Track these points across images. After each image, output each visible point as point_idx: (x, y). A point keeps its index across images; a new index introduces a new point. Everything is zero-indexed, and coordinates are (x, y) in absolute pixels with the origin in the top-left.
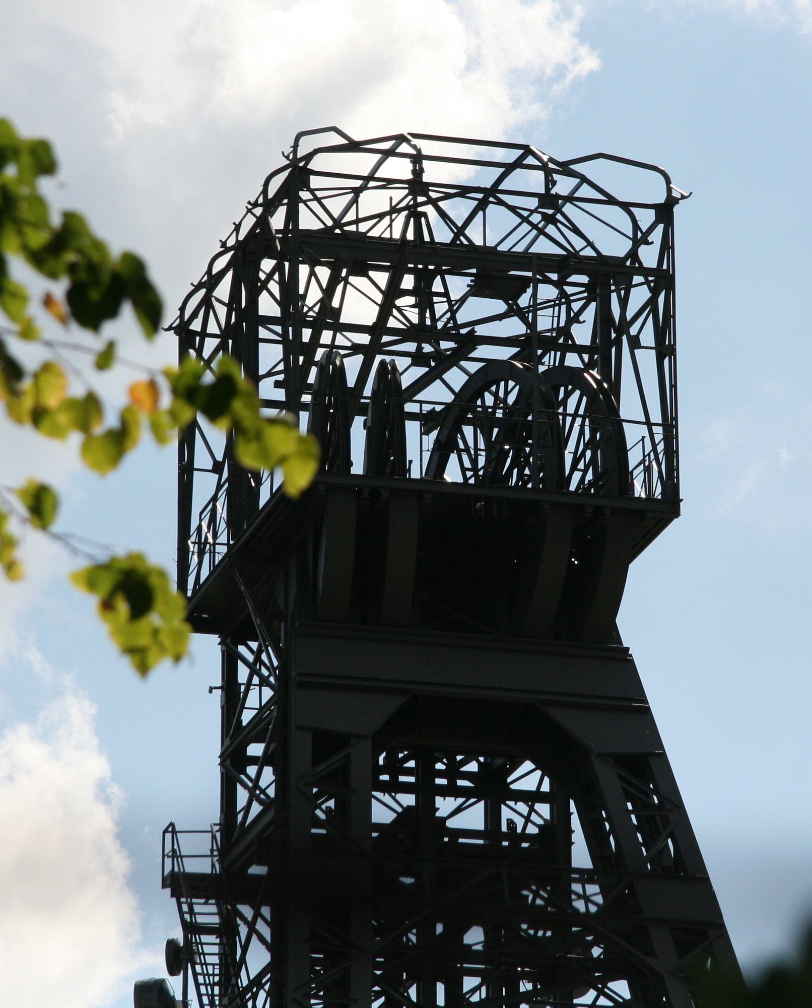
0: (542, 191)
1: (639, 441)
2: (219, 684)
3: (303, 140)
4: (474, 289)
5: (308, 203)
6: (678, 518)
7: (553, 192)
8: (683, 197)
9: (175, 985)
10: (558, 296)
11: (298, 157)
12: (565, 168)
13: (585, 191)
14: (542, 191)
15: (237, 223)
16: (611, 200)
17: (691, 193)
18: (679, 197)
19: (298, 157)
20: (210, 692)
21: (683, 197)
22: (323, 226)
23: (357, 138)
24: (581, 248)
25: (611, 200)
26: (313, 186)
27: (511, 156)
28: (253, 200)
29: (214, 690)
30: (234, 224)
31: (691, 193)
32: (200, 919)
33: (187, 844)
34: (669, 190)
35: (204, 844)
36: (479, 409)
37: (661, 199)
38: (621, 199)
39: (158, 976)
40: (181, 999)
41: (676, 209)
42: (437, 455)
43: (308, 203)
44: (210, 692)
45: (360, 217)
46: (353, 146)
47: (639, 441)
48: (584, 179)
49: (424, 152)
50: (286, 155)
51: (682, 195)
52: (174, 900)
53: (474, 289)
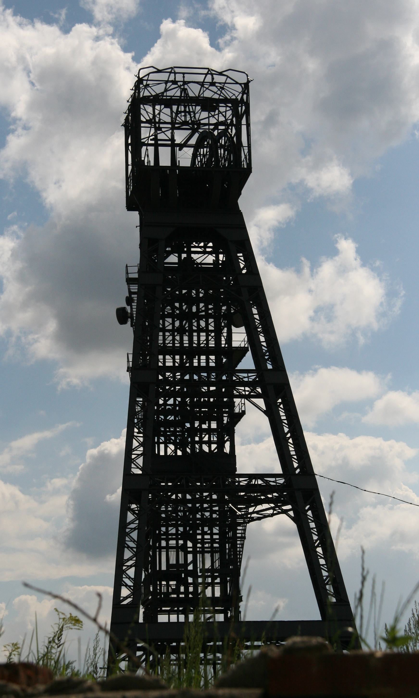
0: (211, 81)
1: (233, 94)
2: (139, 225)
3: (141, 71)
4: (170, 505)
5: (151, 87)
6: (252, 171)
7: (214, 81)
8: (251, 80)
9: (128, 309)
10: (151, 107)
11: (205, 75)
12: (221, 74)
13: (229, 81)
14: (211, 81)
15: (132, 95)
16: (237, 83)
17: (253, 79)
18: (250, 80)
19: (205, 75)
20: (136, 227)
21: (251, 80)
22: (156, 94)
23: (160, 68)
24: (231, 96)
25: (237, 83)
26: (216, 85)
27: (206, 71)
28: (131, 88)
29: (137, 227)
30: (131, 95)
31: (253, 79)
32: (132, 290)
33: (130, 270)
34: (248, 79)
35: (136, 269)
36: (219, 146)
37: (245, 81)
38: (239, 82)
39: (123, 306)
40: (130, 312)
41: (250, 84)
42: (193, 157)
43: (151, 87)
44: (136, 227)
45: (214, 93)
46: (159, 71)
47: (233, 94)
48: (228, 77)
49: (176, 72)
50: (135, 75)
51: (251, 80)
52: (127, 285)
53: (170, 505)
